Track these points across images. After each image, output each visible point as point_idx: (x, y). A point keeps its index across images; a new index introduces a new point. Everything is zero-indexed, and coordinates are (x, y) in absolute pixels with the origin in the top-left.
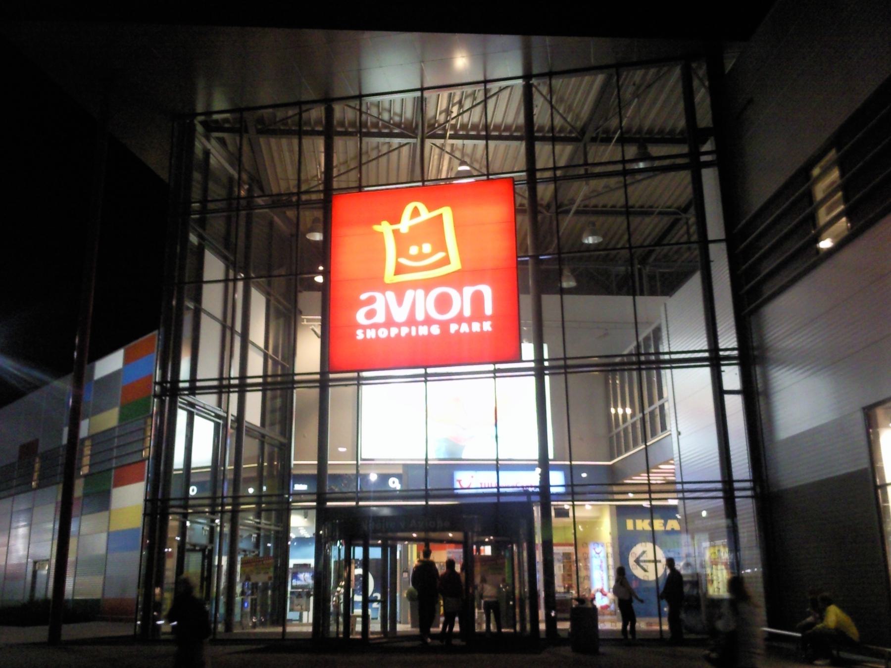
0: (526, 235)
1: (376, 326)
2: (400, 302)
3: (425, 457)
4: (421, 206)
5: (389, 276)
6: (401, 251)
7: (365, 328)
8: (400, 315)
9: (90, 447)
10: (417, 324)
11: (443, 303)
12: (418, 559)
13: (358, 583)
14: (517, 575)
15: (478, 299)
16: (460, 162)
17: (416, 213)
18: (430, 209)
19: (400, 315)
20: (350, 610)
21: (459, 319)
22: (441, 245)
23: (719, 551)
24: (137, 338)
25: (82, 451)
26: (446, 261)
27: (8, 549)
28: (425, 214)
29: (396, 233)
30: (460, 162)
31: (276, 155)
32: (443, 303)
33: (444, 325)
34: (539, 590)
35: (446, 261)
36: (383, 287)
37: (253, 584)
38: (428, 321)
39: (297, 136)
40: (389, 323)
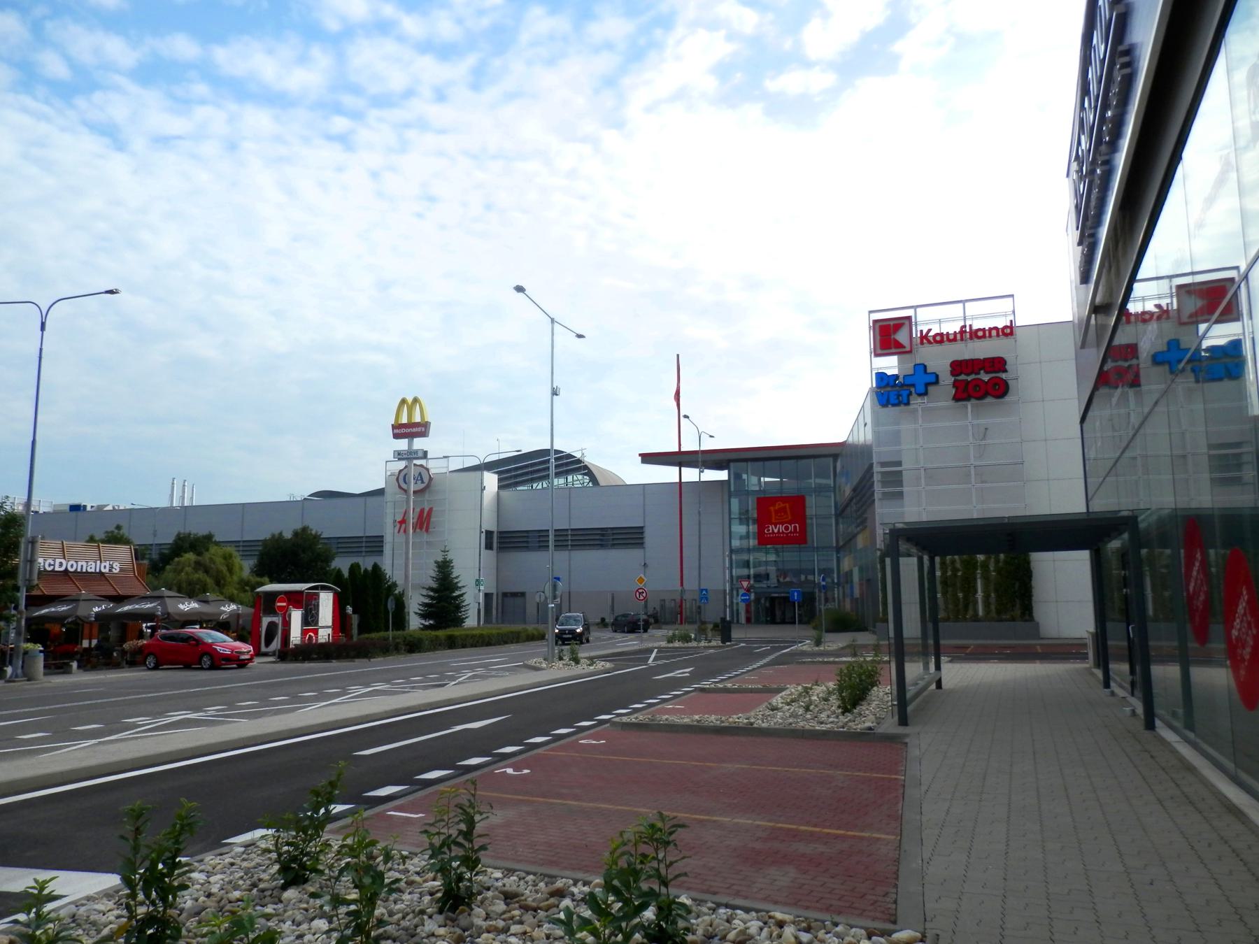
1: (770, 534)
3: (1012, 309)
4: (781, 504)
5: (773, 521)
8: (776, 531)
9: (81, 102)
10: (780, 533)
11: (787, 528)
12: (497, 63)
14: (253, 548)
15: (795, 527)
17: (779, 504)
19: (776, 531)
20: (883, 611)
21: (791, 532)
25: (51, 607)
28: (782, 505)
32: (787, 528)
33: (787, 534)
34: (354, 662)
37: (716, 626)
39: (733, 548)
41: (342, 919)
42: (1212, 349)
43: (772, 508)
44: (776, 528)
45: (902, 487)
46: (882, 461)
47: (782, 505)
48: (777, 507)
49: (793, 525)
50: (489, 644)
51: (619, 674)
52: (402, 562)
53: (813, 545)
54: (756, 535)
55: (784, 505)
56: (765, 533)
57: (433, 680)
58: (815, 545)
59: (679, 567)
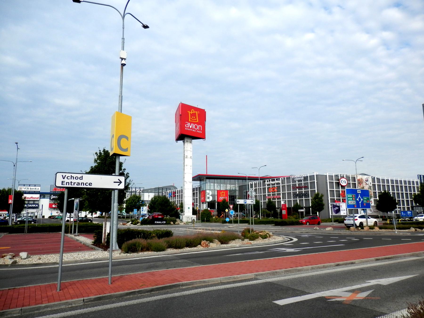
0: (375, 281)
1: (187, 128)
2: (191, 125)
5: (190, 121)
6: (191, 117)
7: (186, 128)
8: (191, 127)
11: (196, 127)
13: (196, 232)
16: (123, 67)
17: (193, 111)
18: (195, 111)
21: (198, 130)
22: (196, 118)
23: (308, 316)
24: (19, 233)
26: (196, 120)
27: (19, 294)
29: (190, 113)
30: (123, 67)
31: (279, 250)
32: (196, 127)
33: (196, 130)
35: (196, 120)
36: (189, 122)
38: (194, 129)
40: (189, 128)
41: (210, 187)
42: (88, 211)
43: (221, 193)
44: (191, 125)
45: (239, 223)
46: (128, 149)
47: (194, 112)
48: (191, 113)
49: (199, 126)
50: (175, 253)
51: (311, 247)
52: (208, 186)
53: (208, 184)
54: (35, 226)
55: (195, 112)
56: (148, 218)
57: (310, 230)
58: (207, 184)
59: (135, 17)
